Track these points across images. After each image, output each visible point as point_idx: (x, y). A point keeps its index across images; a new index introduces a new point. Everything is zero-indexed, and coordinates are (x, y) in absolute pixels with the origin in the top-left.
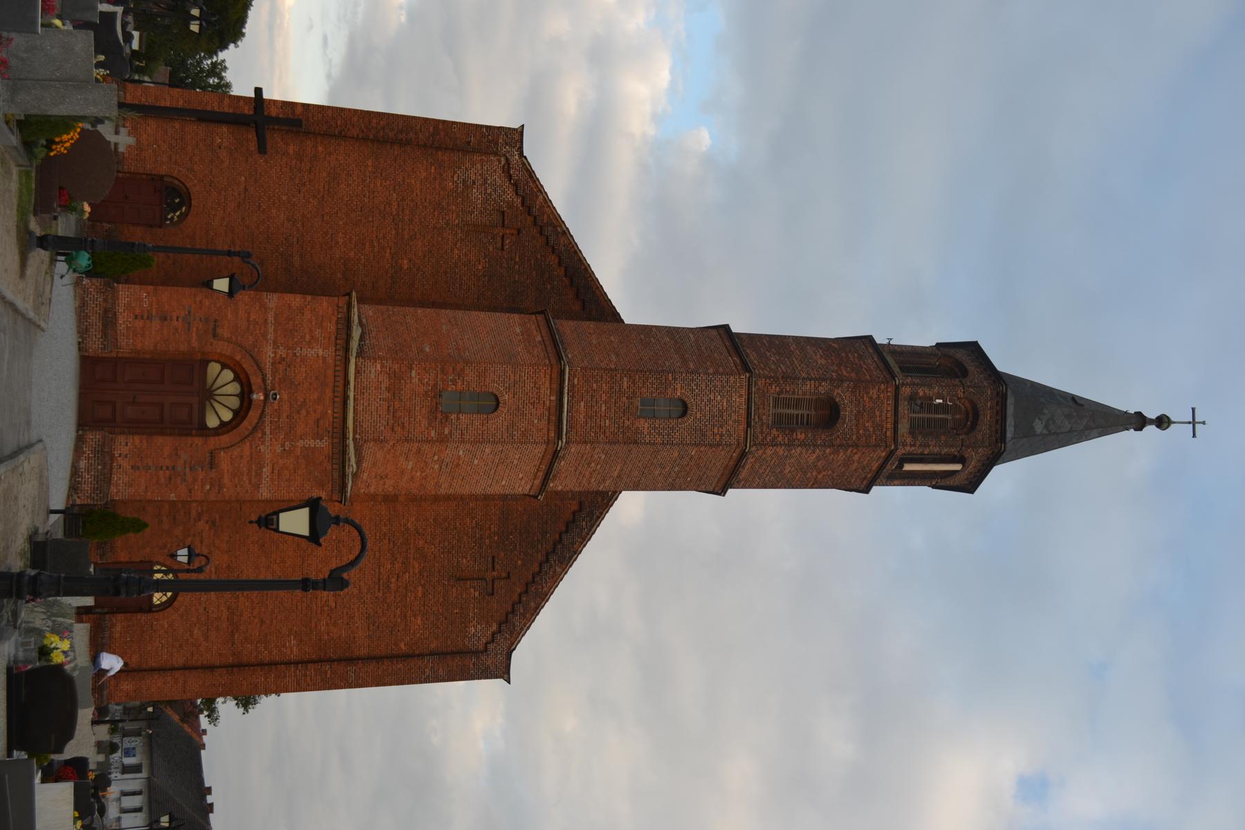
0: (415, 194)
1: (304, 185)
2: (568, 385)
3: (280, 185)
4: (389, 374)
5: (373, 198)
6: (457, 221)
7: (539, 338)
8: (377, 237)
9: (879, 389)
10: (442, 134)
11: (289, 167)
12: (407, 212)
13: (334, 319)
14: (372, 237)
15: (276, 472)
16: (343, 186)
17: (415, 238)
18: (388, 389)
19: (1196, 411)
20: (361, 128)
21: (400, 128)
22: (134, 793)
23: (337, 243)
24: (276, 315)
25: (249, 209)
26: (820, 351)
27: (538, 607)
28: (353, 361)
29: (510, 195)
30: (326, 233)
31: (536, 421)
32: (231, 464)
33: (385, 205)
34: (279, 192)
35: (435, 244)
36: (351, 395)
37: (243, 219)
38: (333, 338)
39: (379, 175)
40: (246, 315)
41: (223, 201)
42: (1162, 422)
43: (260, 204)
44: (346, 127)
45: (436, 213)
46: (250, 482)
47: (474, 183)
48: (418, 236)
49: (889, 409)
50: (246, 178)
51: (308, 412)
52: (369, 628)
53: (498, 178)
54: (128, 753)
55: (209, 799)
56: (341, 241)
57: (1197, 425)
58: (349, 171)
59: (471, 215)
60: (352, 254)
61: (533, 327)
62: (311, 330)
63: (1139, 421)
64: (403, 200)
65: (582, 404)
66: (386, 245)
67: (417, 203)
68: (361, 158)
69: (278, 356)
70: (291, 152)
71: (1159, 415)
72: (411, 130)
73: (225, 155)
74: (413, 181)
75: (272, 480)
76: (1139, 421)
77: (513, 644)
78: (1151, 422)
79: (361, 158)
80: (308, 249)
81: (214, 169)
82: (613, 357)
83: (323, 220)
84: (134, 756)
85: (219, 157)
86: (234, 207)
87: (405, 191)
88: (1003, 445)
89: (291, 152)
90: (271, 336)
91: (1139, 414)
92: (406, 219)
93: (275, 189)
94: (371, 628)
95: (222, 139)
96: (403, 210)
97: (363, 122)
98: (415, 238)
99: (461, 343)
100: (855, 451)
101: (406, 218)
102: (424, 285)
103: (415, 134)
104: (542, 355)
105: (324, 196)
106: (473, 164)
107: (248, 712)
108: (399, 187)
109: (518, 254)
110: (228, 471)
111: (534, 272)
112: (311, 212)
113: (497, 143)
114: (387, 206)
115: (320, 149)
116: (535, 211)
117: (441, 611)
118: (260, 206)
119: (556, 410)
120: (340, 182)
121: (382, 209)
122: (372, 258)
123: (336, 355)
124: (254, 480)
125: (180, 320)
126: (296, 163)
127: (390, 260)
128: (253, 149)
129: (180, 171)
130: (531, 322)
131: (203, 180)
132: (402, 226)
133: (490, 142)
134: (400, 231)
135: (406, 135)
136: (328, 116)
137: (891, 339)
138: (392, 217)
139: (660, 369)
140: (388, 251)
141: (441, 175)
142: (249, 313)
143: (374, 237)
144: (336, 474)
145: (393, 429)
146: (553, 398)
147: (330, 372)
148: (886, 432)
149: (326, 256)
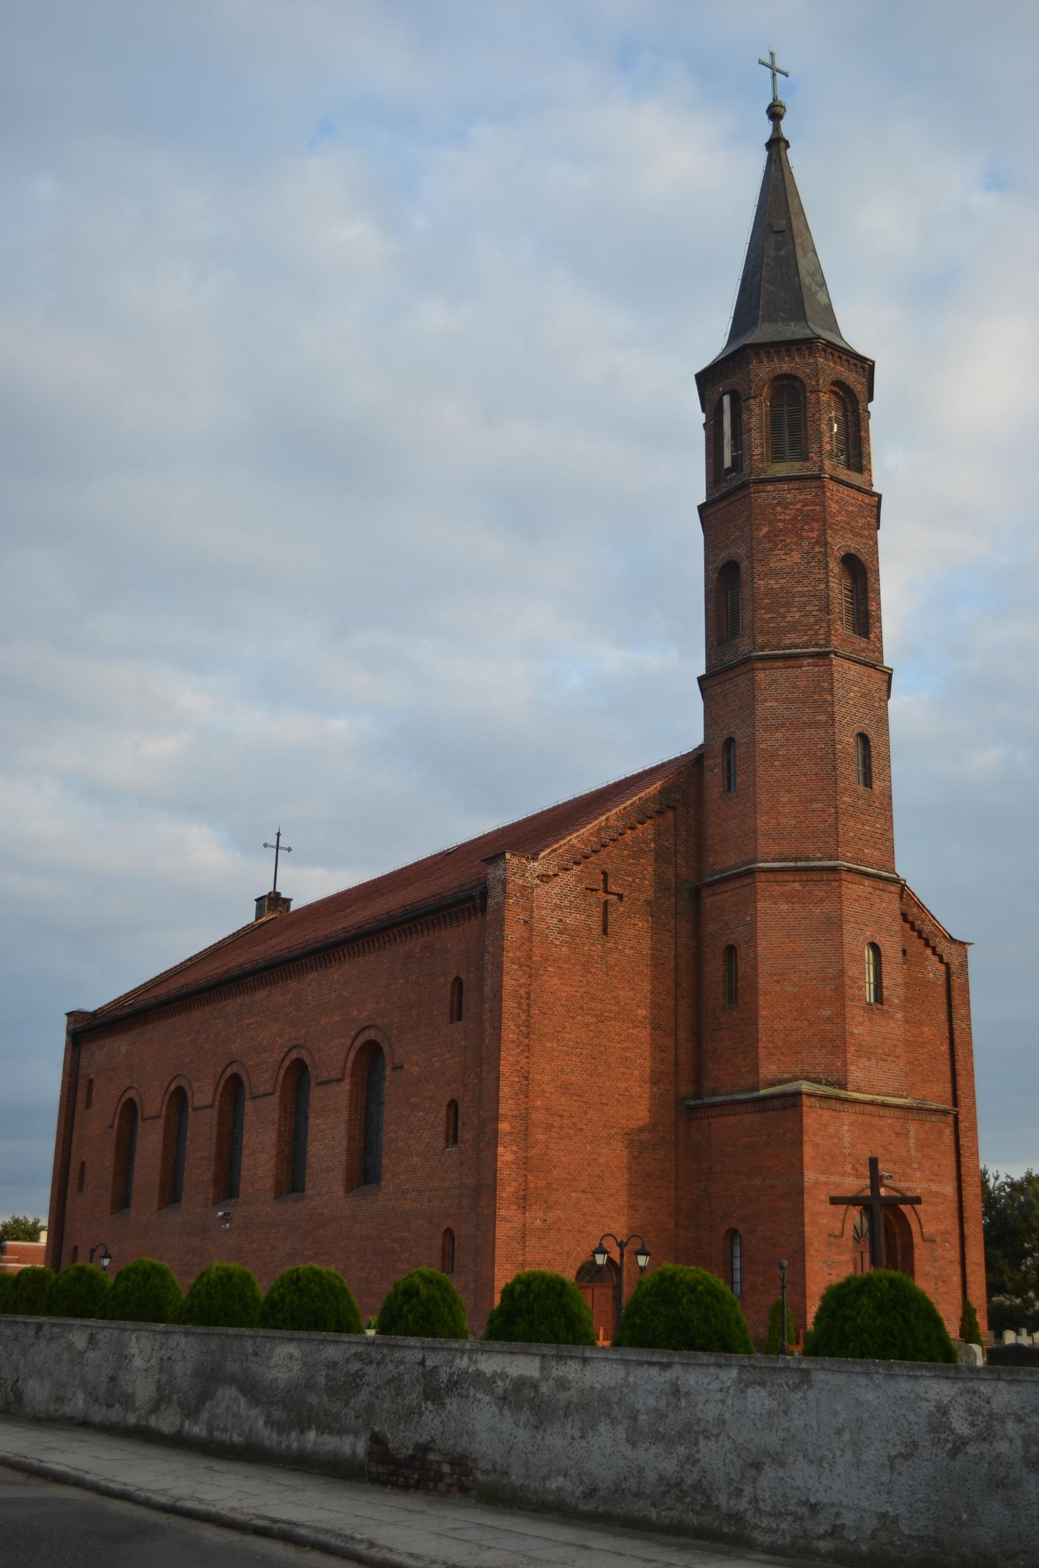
1: (575, 1124)
2: (852, 863)
3: (577, 1152)
4: (858, 1057)
5: (582, 1043)
7: (797, 886)
8: (619, 1043)
9: (830, 498)
10: (518, 954)
11: (559, 1141)
12: (593, 1004)
13: (820, 1111)
16: (573, 1079)
17: (617, 998)
18: (869, 1059)
19: (784, 77)
23: (626, 1089)
24: (822, 1173)
25: (601, 1188)
27: (918, 904)
30: (619, 1101)
32: (930, 1221)
33: (589, 1030)
35: (621, 974)
37: (611, 1195)
38: (834, 1114)
39: (560, 1035)
40: (823, 1203)
41: (595, 1218)
42: (775, 113)
44: (520, 1071)
45: (593, 970)
46: (942, 1203)
48: (615, 994)
49: (846, 493)
50: (574, 1191)
51: (891, 1144)
52: (931, 1081)
53: (553, 889)
59: (592, 928)
60: (636, 1073)
61: (778, 888)
62: (830, 1137)
63: (776, 145)
64: (581, 1008)
65: (866, 851)
66: (626, 1032)
68: (545, 1055)
69: (851, 1172)
71: (766, 117)
74: (564, 994)
76: (776, 145)
78: (777, 128)
79: (545, 1055)
82: (815, 806)
85: (555, 1223)
87: (574, 1005)
88: (868, 362)
94: (931, 1079)
95: (536, 1218)
96: (593, 1010)
98: (617, 998)
99: (813, 974)
102: (659, 993)
105: (583, 1102)
106: (542, 919)
109: (626, 878)
110: (936, 1225)
111: (641, 860)
113: (524, 887)
114: (590, 1028)
116: (587, 851)
117: (918, 1006)
118: (598, 1176)
119: (874, 881)
121: (592, 1034)
123: (848, 1112)
126: (556, 1132)
127: (639, 1030)
128: (544, 1182)
129: (571, 1267)
131: (578, 1241)
132: (607, 1012)
133: (523, 896)
134: (612, 1015)
135: (522, 998)
138: (600, 1024)
140: (631, 1031)
142: (821, 1201)
143: (619, 1045)
144: (934, 1118)
145: (898, 1057)
146: (866, 883)
147: (860, 1118)
148: (865, 503)
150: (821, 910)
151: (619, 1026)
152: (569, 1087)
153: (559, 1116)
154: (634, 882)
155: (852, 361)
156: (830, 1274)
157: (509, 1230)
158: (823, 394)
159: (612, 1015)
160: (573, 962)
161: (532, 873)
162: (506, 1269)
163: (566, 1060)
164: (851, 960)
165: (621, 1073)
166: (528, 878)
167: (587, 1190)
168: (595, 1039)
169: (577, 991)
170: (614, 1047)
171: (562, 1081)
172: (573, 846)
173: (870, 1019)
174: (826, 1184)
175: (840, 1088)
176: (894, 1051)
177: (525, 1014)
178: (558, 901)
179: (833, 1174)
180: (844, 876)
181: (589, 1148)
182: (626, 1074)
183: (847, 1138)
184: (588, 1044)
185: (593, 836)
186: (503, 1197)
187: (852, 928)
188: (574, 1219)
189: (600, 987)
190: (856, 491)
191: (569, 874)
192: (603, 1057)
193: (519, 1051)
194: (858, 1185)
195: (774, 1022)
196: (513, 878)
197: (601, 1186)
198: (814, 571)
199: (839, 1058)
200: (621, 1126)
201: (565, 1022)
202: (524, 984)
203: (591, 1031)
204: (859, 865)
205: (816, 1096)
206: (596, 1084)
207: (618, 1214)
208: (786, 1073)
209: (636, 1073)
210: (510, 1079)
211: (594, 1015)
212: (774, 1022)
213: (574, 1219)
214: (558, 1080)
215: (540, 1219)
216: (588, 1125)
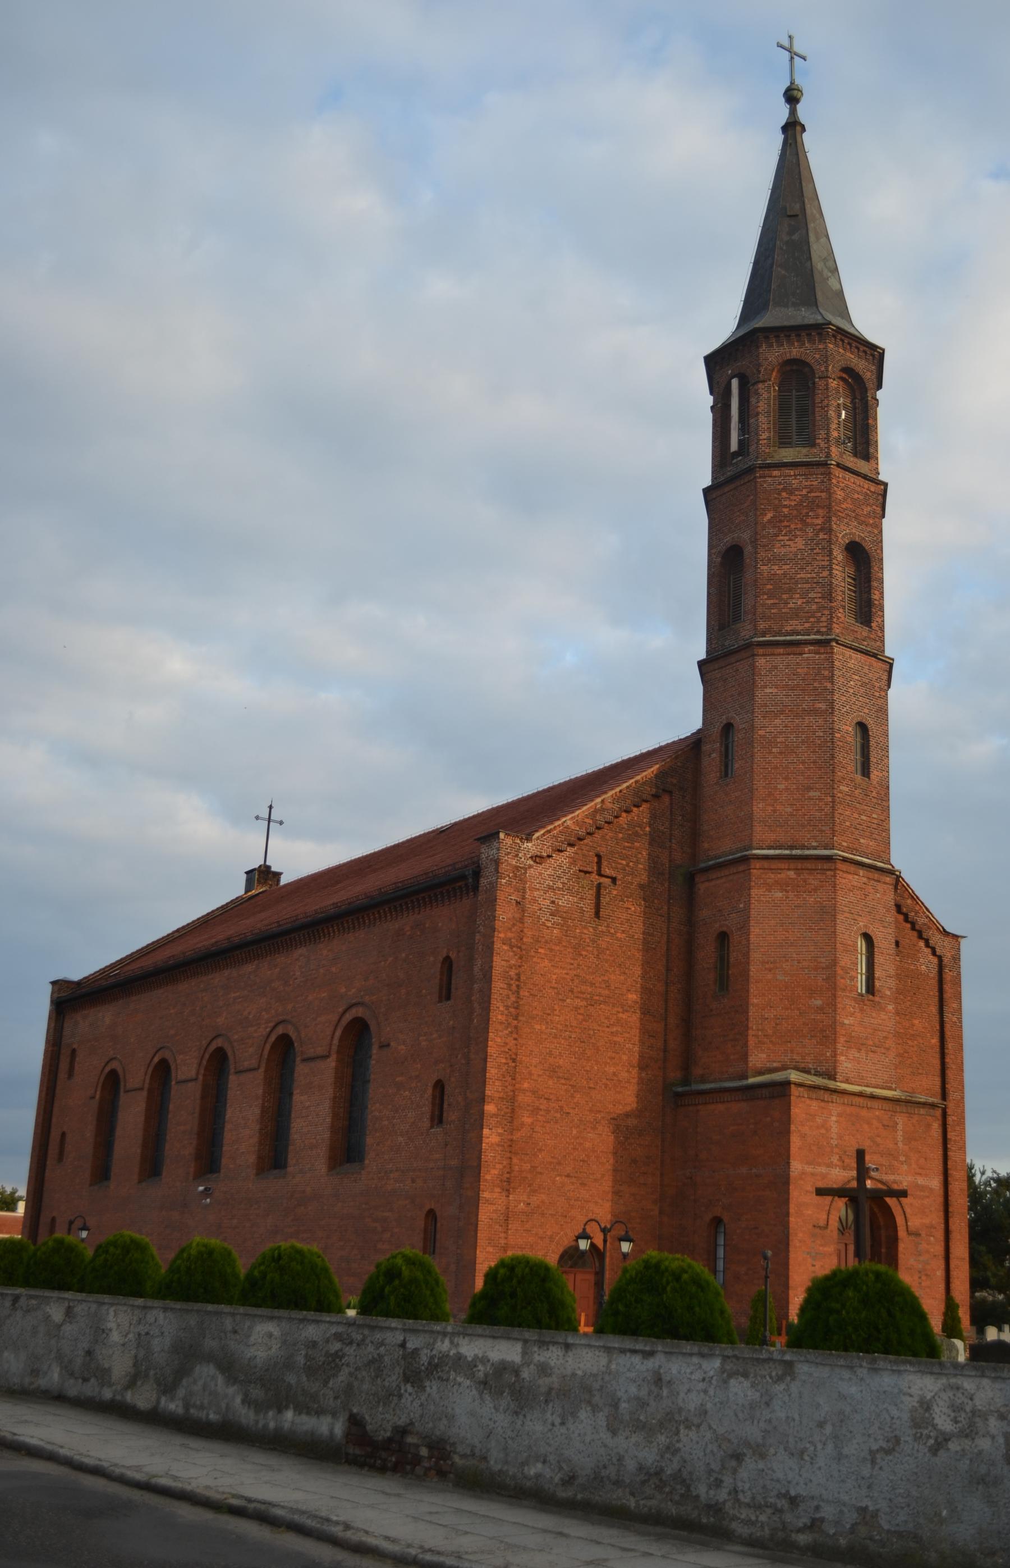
0: (566, 976)
1: (561, 1108)
2: (847, 853)
3: (563, 1135)
5: (572, 1026)
8: (608, 1027)
11: (545, 1124)
12: (583, 988)
13: (808, 1102)
14: (608, 1032)
16: (561, 1062)
18: (859, 1050)
19: (803, 60)
20: (507, 1035)
21: (505, 986)
23: (614, 1074)
24: (809, 1163)
26: (781, 538)
29: (562, 859)
31: (878, 895)
34: (569, 1137)
37: (596, 1180)
38: (822, 1104)
39: (549, 1017)
41: (579, 1203)
43: (581, 1161)
44: (508, 1052)
45: (584, 953)
47: (553, 902)
48: (606, 978)
50: (559, 1175)
58: (547, 1054)
59: (584, 911)
60: (625, 1058)
61: (772, 876)
63: (792, 129)
64: (572, 991)
65: (862, 841)
67: (575, 975)
68: (534, 1037)
70: (529, 1120)
71: (783, 100)
72: (508, 972)
73: (535, 1198)
74: (554, 977)
76: (792, 129)
77: (938, 928)
78: (793, 112)
80: (621, 1107)
81: (550, 1212)
82: (812, 794)
83: (594, 1088)
85: (538, 1207)
86: (584, 1190)
88: (878, 350)
89: (529, 1120)
90: (823, 1170)
92: (590, 990)
93: (567, 1143)
94: (920, 1071)
97: (502, 1031)
102: (650, 977)
103: (512, 968)
104: (819, 876)
106: (534, 900)
108: (559, 994)
109: (620, 861)
110: (921, 1218)
112: (587, 1102)
114: (579, 1011)
116: (582, 833)
118: (583, 1161)
120: (557, 1065)
121: (581, 1017)
122: (627, 1035)
124: (927, 1194)
126: (542, 1115)
130: (763, 876)
131: (561, 1225)
133: (515, 876)
134: (601, 999)
135: (512, 979)
136: (497, 1074)
138: (589, 1007)
139: (829, 744)
140: (621, 1015)
142: (807, 1191)
143: (608, 1030)
144: (922, 1111)
146: (861, 873)
147: (848, 1110)
149: (627, 1087)
150: (815, 899)
153: (546, 1099)
154: (628, 865)
155: (862, 348)
157: (492, 1213)
158: (832, 380)
164: (844, 950)
166: (521, 858)
168: (584, 1023)
169: (567, 974)
174: (812, 1174)
178: (551, 883)
179: (819, 1165)
181: (575, 1132)
182: (614, 1058)
183: (835, 1129)
186: (486, 1180)
193: (507, 1032)
194: (844, 1176)
196: (506, 858)
200: (607, 1110)
202: (514, 965)
211: (584, 998)
215: (524, 1202)
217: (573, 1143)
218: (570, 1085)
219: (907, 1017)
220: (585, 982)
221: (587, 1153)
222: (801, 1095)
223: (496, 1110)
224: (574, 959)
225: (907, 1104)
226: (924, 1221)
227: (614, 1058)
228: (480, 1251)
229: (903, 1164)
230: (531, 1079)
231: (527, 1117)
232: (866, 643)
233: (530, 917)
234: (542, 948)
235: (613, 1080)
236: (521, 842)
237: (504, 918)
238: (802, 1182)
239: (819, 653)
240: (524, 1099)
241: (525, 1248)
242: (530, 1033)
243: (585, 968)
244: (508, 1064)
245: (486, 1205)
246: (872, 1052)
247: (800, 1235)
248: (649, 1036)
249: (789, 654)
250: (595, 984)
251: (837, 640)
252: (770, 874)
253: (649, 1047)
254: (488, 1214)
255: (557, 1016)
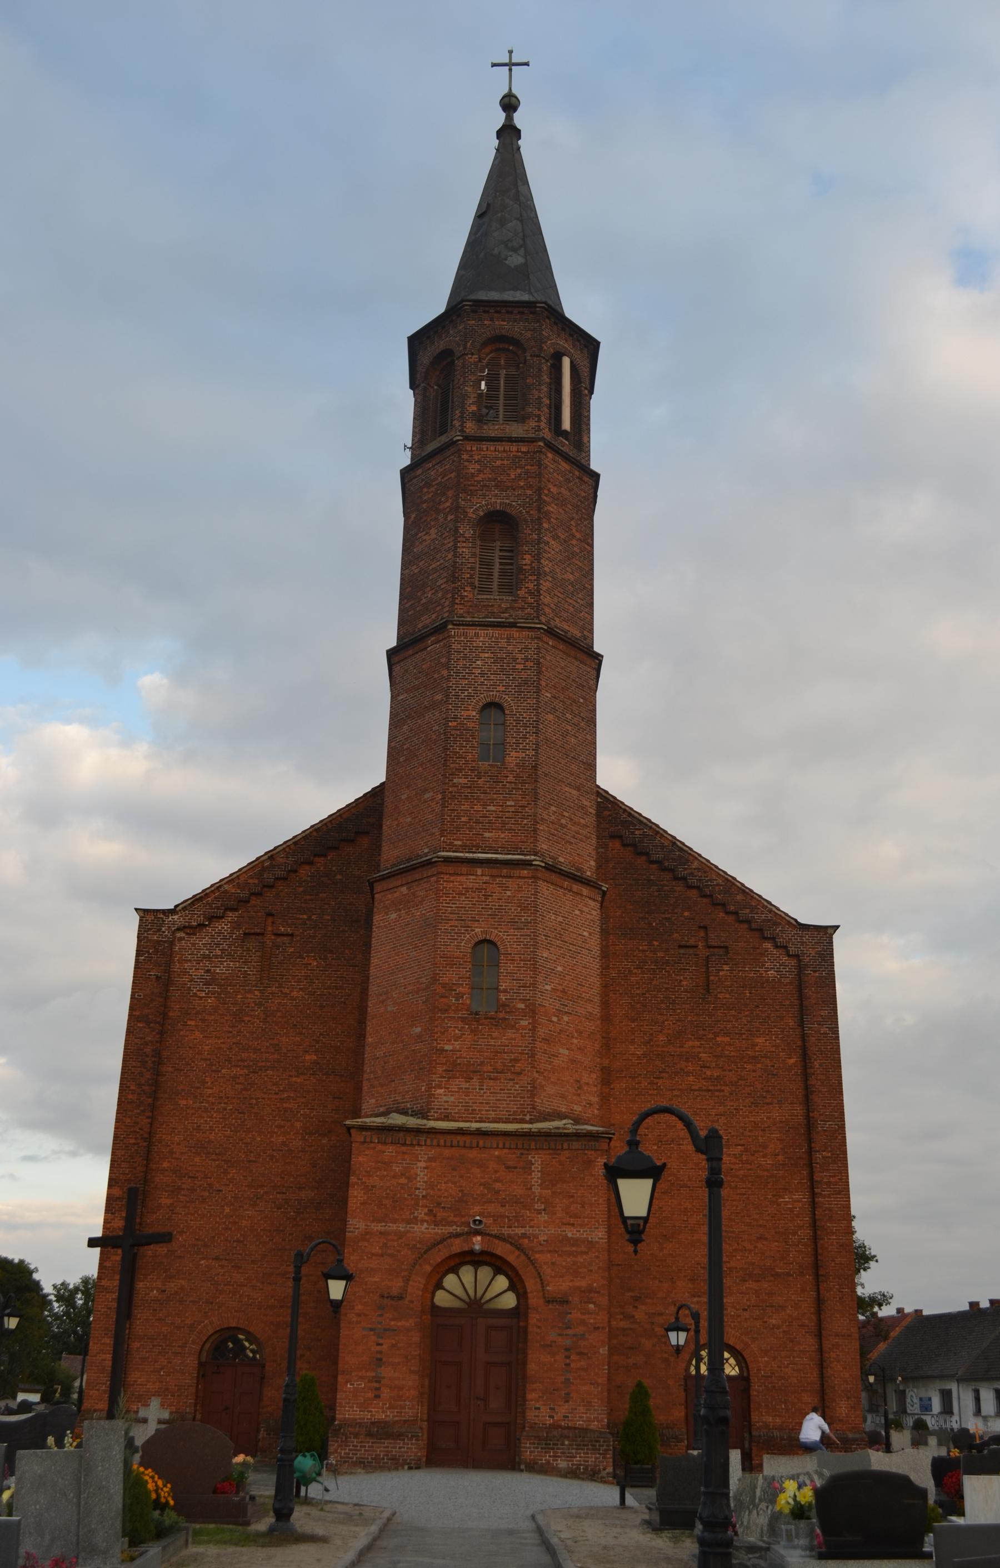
0: (223, 1046)
1: (210, 1185)
2: (462, 852)
3: (211, 1215)
6: (256, 993)
7: (404, 889)
8: (276, 1093)
9: (468, 461)
10: (146, 1011)
11: (188, 1205)
13: (380, 1147)
15: (572, 1220)
16: (212, 1137)
18: (469, 1079)
19: (526, 67)
21: (139, 1064)
22: (978, 1400)
23: (283, 1143)
25: (241, 1255)
28: (432, 1124)
29: (224, 926)
30: (272, 1157)
31: (509, 893)
32: (562, 1276)
36: (475, 1126)
37: (253, 1262)
38: (404, 1149)
39: (198, 1091)
40: (374, 1258)
41: (231, 1287)
42: (509, 104)
44: (138, 1132)
45: (246, 1019)
46: (586, 1253)
47: (208, 971)
48: (276, 1042)
49: (492, 448)
50: (203, 1259)
51: (497, 1180)
53: (202, 941)
54: (926, 1407)
55: (985, 1304)
56: (281, 1139)
57: (514, 61)
58: (193, 1129)
59: (249, 975)
60: (298, 1125)
61: (390, 896)
62: (394, 1177)
63: (509, 134)
64: (229, 1060)
65: (487, 835)
70: (169, 1201)
71: (500, 109)
74: (206, 1048)
75: (582, 1226)
76: (509, 134)
77: (789, 922)
78: (509, 118)
82: (427, 796)
84: (930, 1399)
88: (538, 305)
89: (169, 1201)
91: (500, 134)
99: (410, 988)
100: (546, 492)
101: (253, 1056)
103: (147, 1044)
104: (425, 885)
105: (224, 1161)
106: (185, 972)
107: (875, 1256)
109: (298, 916)
110: (572, 1281)
113: (158, 942)
114: (237, 1081)
115: (165, 1165)
116: (244, 894)
118: (238, 1241)
120: (207, 1140)
121: (240, 1087)
122: (304, 1100)
124: (583, 1249)
125: (381, 1341)
126: (185, 1195)
131: (205, 1313)
133: (156, 951)
134: (269, 1064)
135: (148, 1056)
137: (405, 446)
141: (198, 1013)
142: (373, 1254)
143: (276, 1097)
144: (576, 1145)
146: (479, 872)
147: (447, 1152)
148: (523, 453)
149: (300, 1157)
150: (421, 912)
151: (277, 1076)
152: (206, 1145)
153: (189, 1177)
154: (309, 919)
156: (378, 1344)
157: (111, 1302)
158: (470, 356)
159: (269, 1064)
160: (221, 1013)
161: (169, 927)
162: (104, 1344)
163: (204, 1117)
164: (447, 964)
165: (276, 1126)
166: (164, 932)
167: (221, 1257)
168: (244, 1092)
169: (224, 1043)
170: (269, 1099)
171: (197, 1140)
172: (226, 892)
173: (472, 1031)
175: (423, 1118)
176: (514, 1066)
177: (149, 1073)
178: (207, 951)
179: (394, 1221)
180: (444, 868)
181: (227, 1210)
182: (284, 1127)
184: (234, 1098)
185: (252, 878)
186: (106, 1267)
187: (451, 926)
188: (202, 1289)
189: (255, 1035)
190: (507, 443)
191: (223, 922)
192: (253, 1111)
193: (138, 1111)
194: (437, 1234)
195: (376, 1049)
196: (146, 935)
197: (241, 1252)
198: (445, 542)
199: (424, 1082)
200: (273, 1184)
201: (206, 1076)
202: (150, 1041)
203: (239, 1083)
204: (475, 853)
205: (373, 1129)
206: (242, 1140)
207: (263, 1283)
208: (381, 1106)
209: (298, 1125)
210: (125, 1141)
211: (244, 1066)
212: (376, 1049)
213: (202, 1289)
214: (192, 1139)
215: (158, 1289)
216: (229, 1185)
217: (225, 1222)
218: (222, 1160)
219: (744, 1037)
220: (247, 1049)
221: (242, 1233)
222: (368, 1140)
223: (121, 1193)
224: (232, 1027)
225: (549, 1138)
226: (577, 1284)
227: (284, 1127)
228: (94, 1343)
229: (541, 1213)
230: (172, 1158)
231: (165, 1198)
232: (506, 615)
233: (177, 990)
234: (192, 1020)
235: (282, 1151)
236: (165, 915)
237: (140, 996)
238: (366, 1244)
239: (440, 641)
240: (162, 1179)
241: (156, 1339)
242: (173, 1109)
243: (248, 1034)
244: (138, 1144)
245: (104, 1294)
246: (490, 1079)
247: (359, 1307)
248: (334, 1098)
249: (417, 653)
250: (260, 1049)
251: (452, 621)
252: (389, 896)
253: (332, 1110)
254: (106, 1303)
255: (209, 1088)
